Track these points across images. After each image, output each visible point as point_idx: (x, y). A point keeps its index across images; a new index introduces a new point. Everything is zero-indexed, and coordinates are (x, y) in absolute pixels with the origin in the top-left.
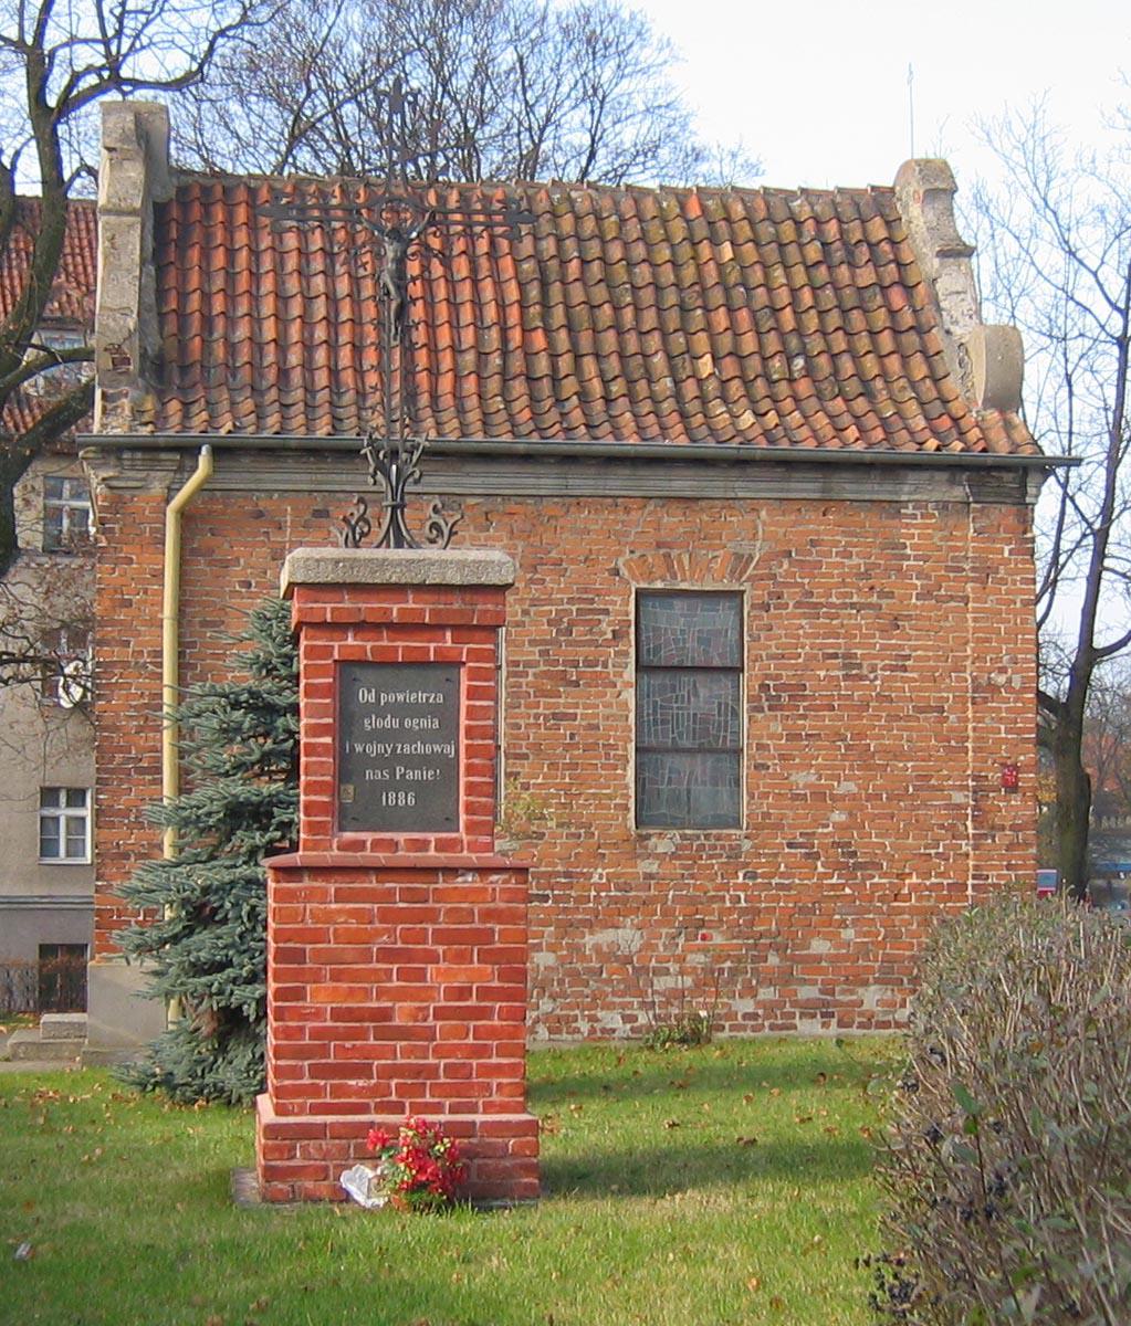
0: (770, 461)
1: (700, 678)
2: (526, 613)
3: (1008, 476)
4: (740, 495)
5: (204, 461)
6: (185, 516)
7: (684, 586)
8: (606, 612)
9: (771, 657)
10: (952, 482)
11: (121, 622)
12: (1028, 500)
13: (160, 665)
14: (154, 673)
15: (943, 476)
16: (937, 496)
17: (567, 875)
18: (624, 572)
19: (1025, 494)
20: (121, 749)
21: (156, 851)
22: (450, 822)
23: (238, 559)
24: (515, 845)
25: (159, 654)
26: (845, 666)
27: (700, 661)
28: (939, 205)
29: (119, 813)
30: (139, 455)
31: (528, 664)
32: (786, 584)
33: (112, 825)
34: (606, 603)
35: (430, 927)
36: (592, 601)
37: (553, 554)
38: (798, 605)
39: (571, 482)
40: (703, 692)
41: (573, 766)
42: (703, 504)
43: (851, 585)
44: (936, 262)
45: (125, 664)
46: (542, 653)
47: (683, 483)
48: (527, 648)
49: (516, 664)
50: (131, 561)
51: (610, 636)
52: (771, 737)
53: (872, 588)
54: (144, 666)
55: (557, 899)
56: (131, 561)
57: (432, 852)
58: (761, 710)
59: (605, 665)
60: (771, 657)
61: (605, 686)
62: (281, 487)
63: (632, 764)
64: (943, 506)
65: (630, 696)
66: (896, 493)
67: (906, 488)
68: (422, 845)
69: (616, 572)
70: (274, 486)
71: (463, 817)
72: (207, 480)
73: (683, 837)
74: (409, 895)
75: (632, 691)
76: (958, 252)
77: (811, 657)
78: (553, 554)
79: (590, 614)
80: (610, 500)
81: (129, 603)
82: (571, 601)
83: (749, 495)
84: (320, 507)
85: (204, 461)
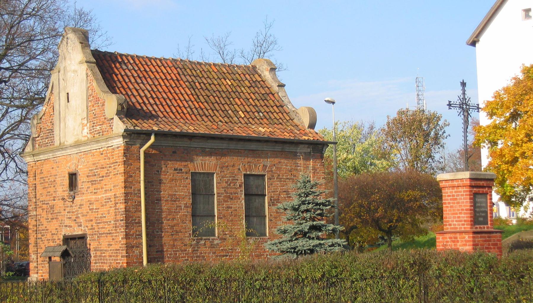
0: (188, 136)
1: (256, 197)
2: (220, 180)
3: (320, 146)
4: (265, 149)
5: (153, 138)
6: (145, 153)
7: (253, 173)
8: (237, 180)
9: (272, 192)
10: (308, 147)
11: (130, 182)
12: (323, 152)
13: (140, 194)
14: (138, 196)
15: (307, 146)
16: (304, 151)
17: (232, 249)
18: (241, 169)
19: (323, 151)
20: (131, 217)
21: (140, 245)
22: (487, 224)
23: (156, 164)
24: (220, 242)
25: (140, 190)
26: (287, 194)
27: (256, 193)
28: (273, 72)
29: (131, 235)
30: (136, 135)
31: (222, 193)
32: (274, 173)
33: (129, 238)
34: (237, 177)
35: (491, 243)
36: (234, 177)
37: (226, 164)
38: (277, 178)
39: (230, 145)
40: (257, 201)
41: (232, 221)
42: (257, 152)
43: (288, 173)
44: (277, 88)
45: (131, 193)
46: (225, 191)
47: (253, 146)
48: (221, 189)
49: (219, 193)
50: (132, 165)
51: (238, 186)
52: (273, 213)
53: (292, 174)
54: (136, 194)
55: (230, 256)
56: (132, 165)
57: (486, 229)
58: (270, 206)
59: (238, 194)
60: (272, 192)
61: (238, 199)
62: (166, 145)
63: (244, 220)
64: (305, 153)
65: (243, 202)
66: (296, 150)
67: (299, 149)
68: (477, 228)
69: (239, 169)
70: (164, 145)
71: (489, 222)
72: (154, 142)
73: (255, 239)
74: (489, 237)
75: (244, 201)
76: (282, 86)
77: (280, 192)
78: (226, 164)
79: (235, 180)
80: (237, 150)
81: (131, 176)
82: (230, 177)
83: (267, 150)
84: (174, 150)
85: (153, 138)
